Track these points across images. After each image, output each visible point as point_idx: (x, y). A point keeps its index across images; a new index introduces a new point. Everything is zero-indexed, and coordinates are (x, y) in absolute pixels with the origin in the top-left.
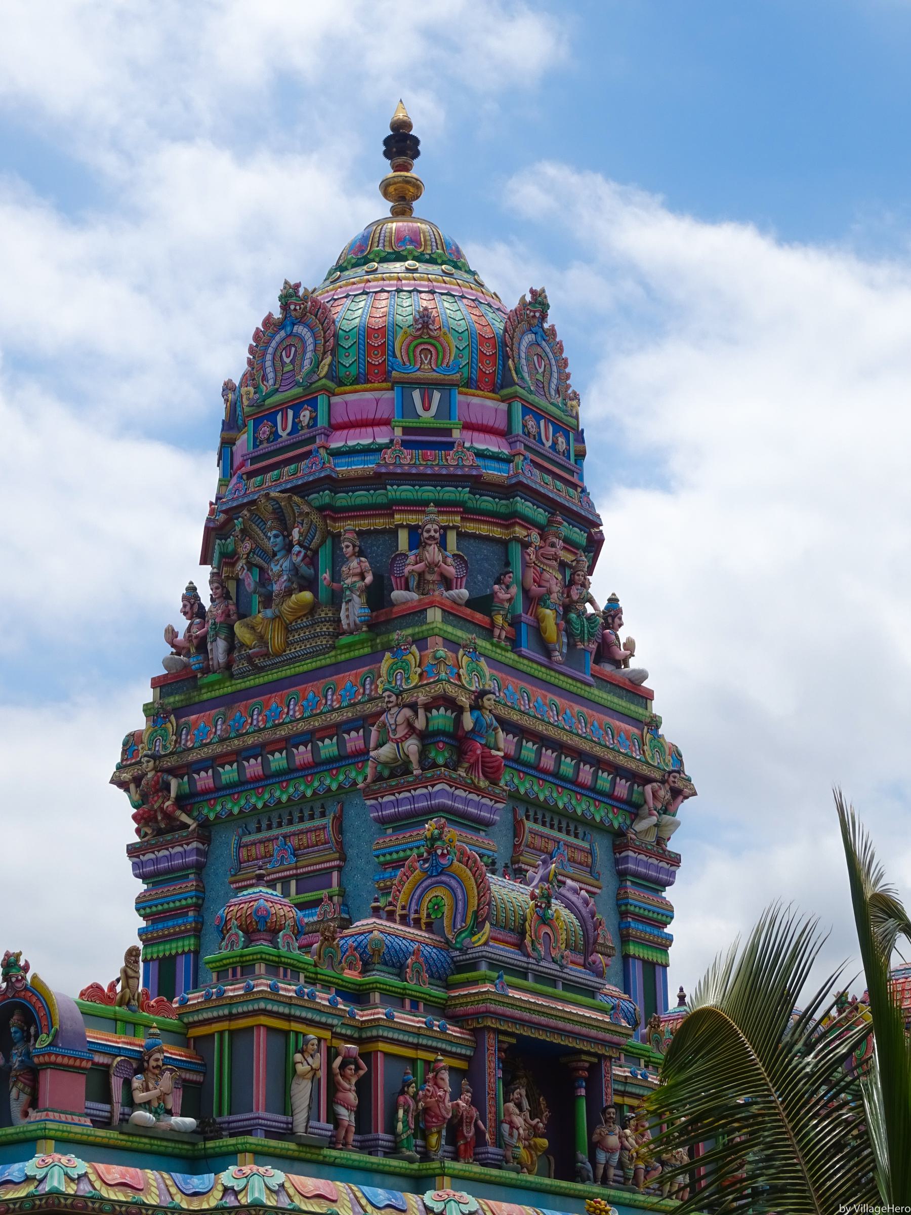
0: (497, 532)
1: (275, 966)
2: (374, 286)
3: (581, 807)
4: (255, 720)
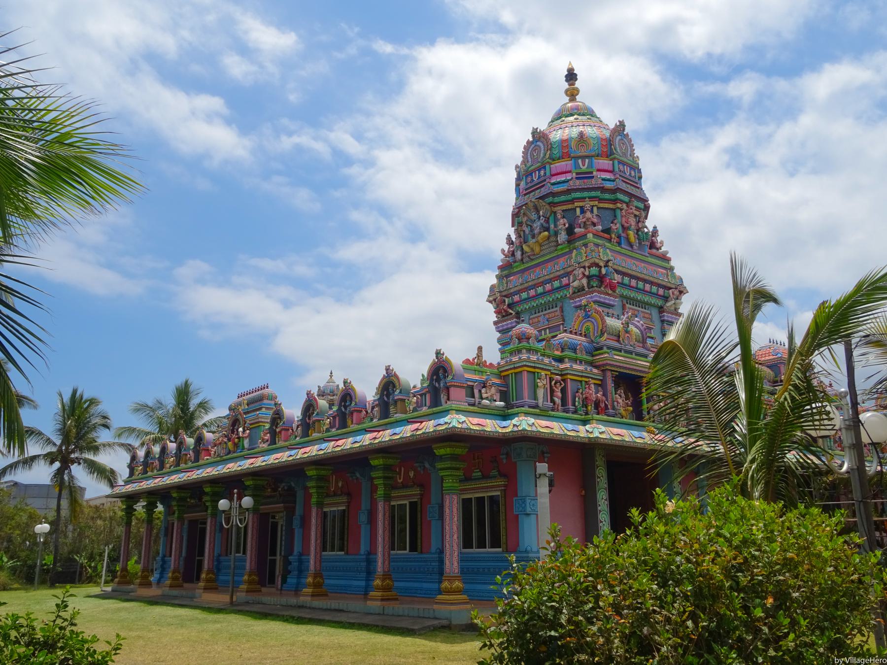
0: (611, 206)
1: (529, 350)
2: (563, 126)
3: (647, 299)
4: (532, 276)
